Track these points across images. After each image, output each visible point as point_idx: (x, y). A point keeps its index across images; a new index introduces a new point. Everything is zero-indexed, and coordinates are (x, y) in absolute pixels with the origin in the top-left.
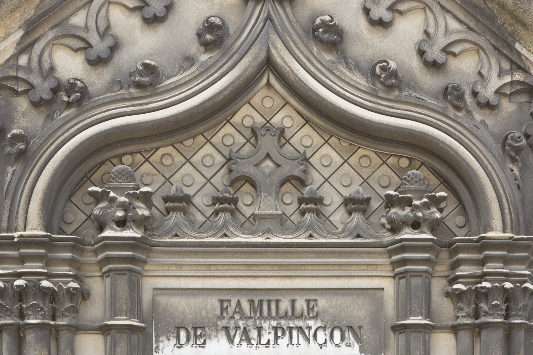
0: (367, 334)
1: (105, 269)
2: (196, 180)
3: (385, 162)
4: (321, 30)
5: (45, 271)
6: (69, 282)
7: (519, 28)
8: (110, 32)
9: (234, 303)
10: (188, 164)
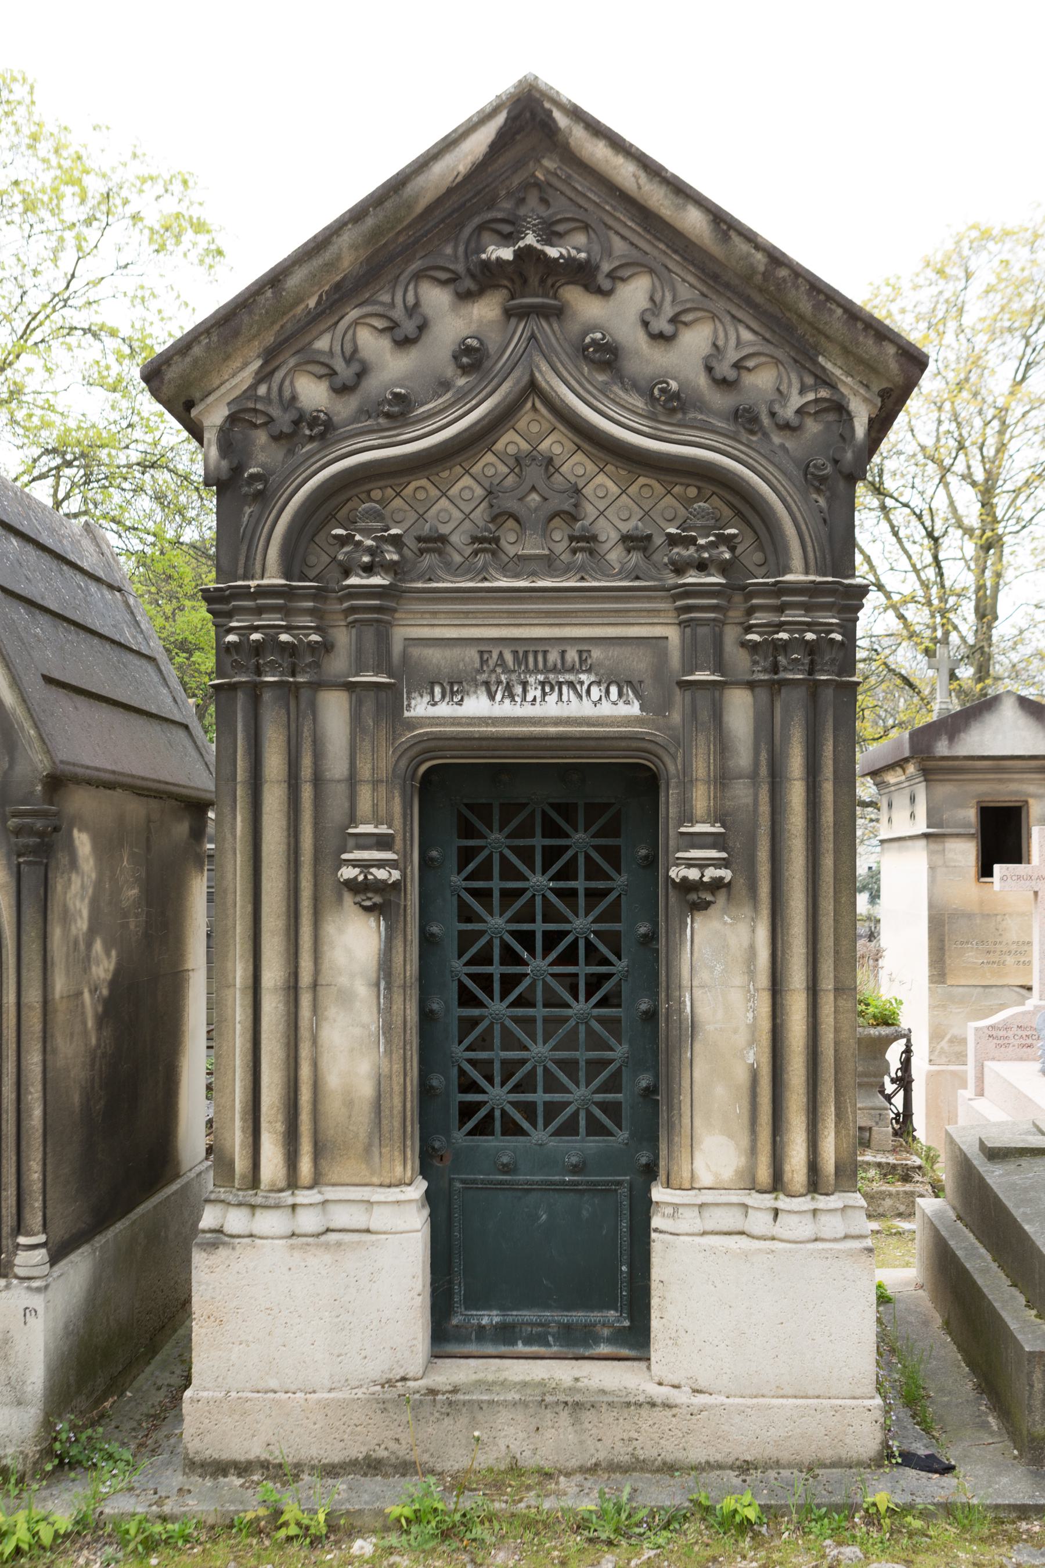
0: (648, 691)
1: (351, 618)
2: (453, 516)
3: (669, 492)
4: (591, 349)
5: (284, 623)
6: (310, 635)
7: (823, 340)
8: (357, 356)
9: (495, 655)
10: (444, 498)
